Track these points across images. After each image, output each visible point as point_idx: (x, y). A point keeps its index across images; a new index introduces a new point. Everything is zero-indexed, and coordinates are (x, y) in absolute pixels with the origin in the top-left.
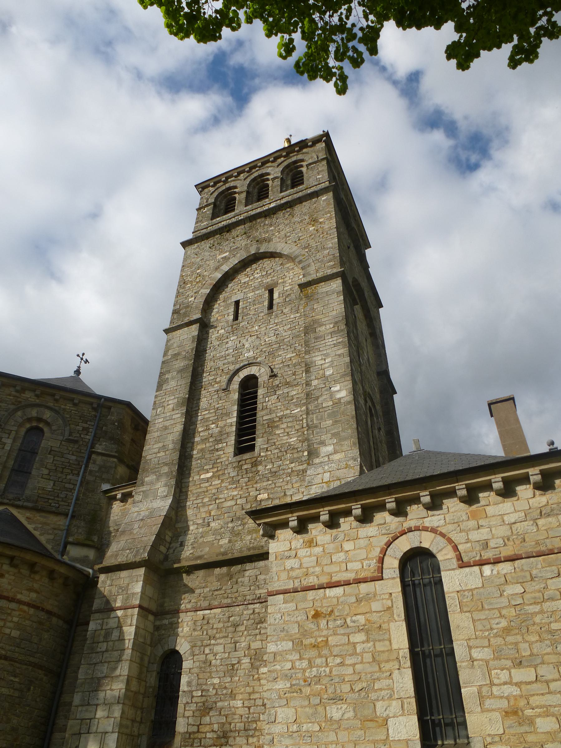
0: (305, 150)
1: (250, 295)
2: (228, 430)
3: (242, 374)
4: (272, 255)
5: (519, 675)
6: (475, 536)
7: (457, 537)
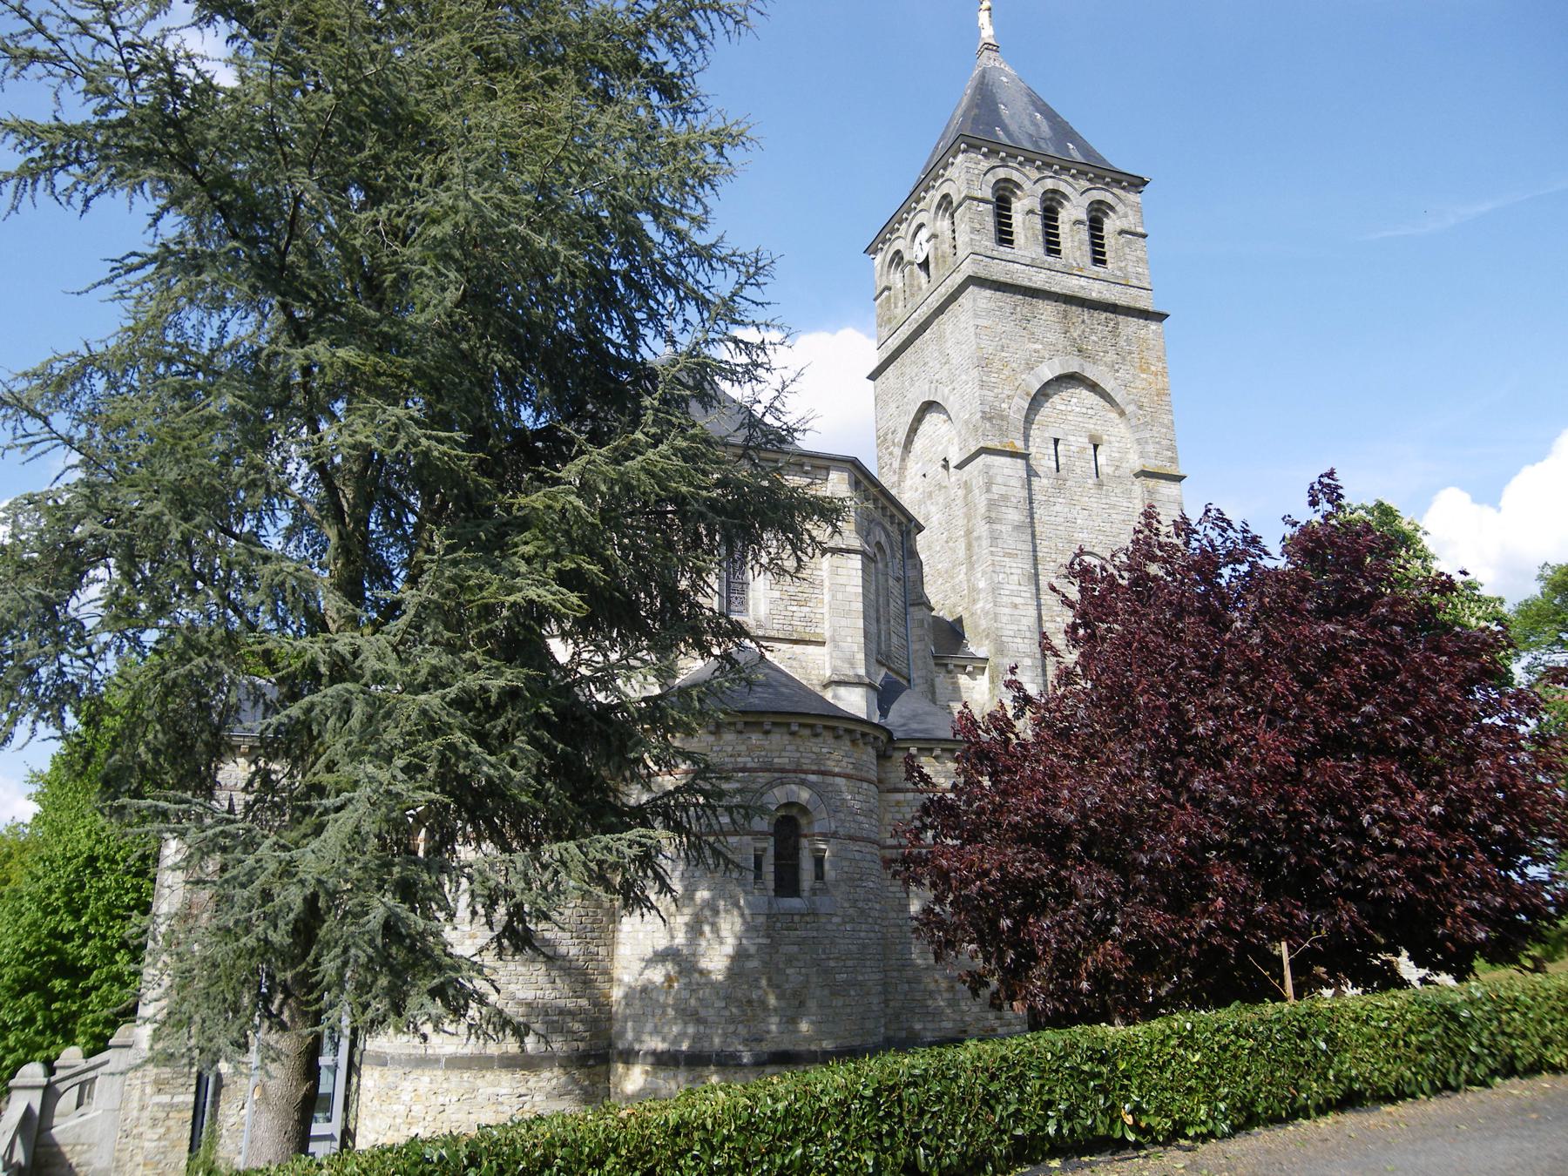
1: (1071, 438)
4: (1093, 387)
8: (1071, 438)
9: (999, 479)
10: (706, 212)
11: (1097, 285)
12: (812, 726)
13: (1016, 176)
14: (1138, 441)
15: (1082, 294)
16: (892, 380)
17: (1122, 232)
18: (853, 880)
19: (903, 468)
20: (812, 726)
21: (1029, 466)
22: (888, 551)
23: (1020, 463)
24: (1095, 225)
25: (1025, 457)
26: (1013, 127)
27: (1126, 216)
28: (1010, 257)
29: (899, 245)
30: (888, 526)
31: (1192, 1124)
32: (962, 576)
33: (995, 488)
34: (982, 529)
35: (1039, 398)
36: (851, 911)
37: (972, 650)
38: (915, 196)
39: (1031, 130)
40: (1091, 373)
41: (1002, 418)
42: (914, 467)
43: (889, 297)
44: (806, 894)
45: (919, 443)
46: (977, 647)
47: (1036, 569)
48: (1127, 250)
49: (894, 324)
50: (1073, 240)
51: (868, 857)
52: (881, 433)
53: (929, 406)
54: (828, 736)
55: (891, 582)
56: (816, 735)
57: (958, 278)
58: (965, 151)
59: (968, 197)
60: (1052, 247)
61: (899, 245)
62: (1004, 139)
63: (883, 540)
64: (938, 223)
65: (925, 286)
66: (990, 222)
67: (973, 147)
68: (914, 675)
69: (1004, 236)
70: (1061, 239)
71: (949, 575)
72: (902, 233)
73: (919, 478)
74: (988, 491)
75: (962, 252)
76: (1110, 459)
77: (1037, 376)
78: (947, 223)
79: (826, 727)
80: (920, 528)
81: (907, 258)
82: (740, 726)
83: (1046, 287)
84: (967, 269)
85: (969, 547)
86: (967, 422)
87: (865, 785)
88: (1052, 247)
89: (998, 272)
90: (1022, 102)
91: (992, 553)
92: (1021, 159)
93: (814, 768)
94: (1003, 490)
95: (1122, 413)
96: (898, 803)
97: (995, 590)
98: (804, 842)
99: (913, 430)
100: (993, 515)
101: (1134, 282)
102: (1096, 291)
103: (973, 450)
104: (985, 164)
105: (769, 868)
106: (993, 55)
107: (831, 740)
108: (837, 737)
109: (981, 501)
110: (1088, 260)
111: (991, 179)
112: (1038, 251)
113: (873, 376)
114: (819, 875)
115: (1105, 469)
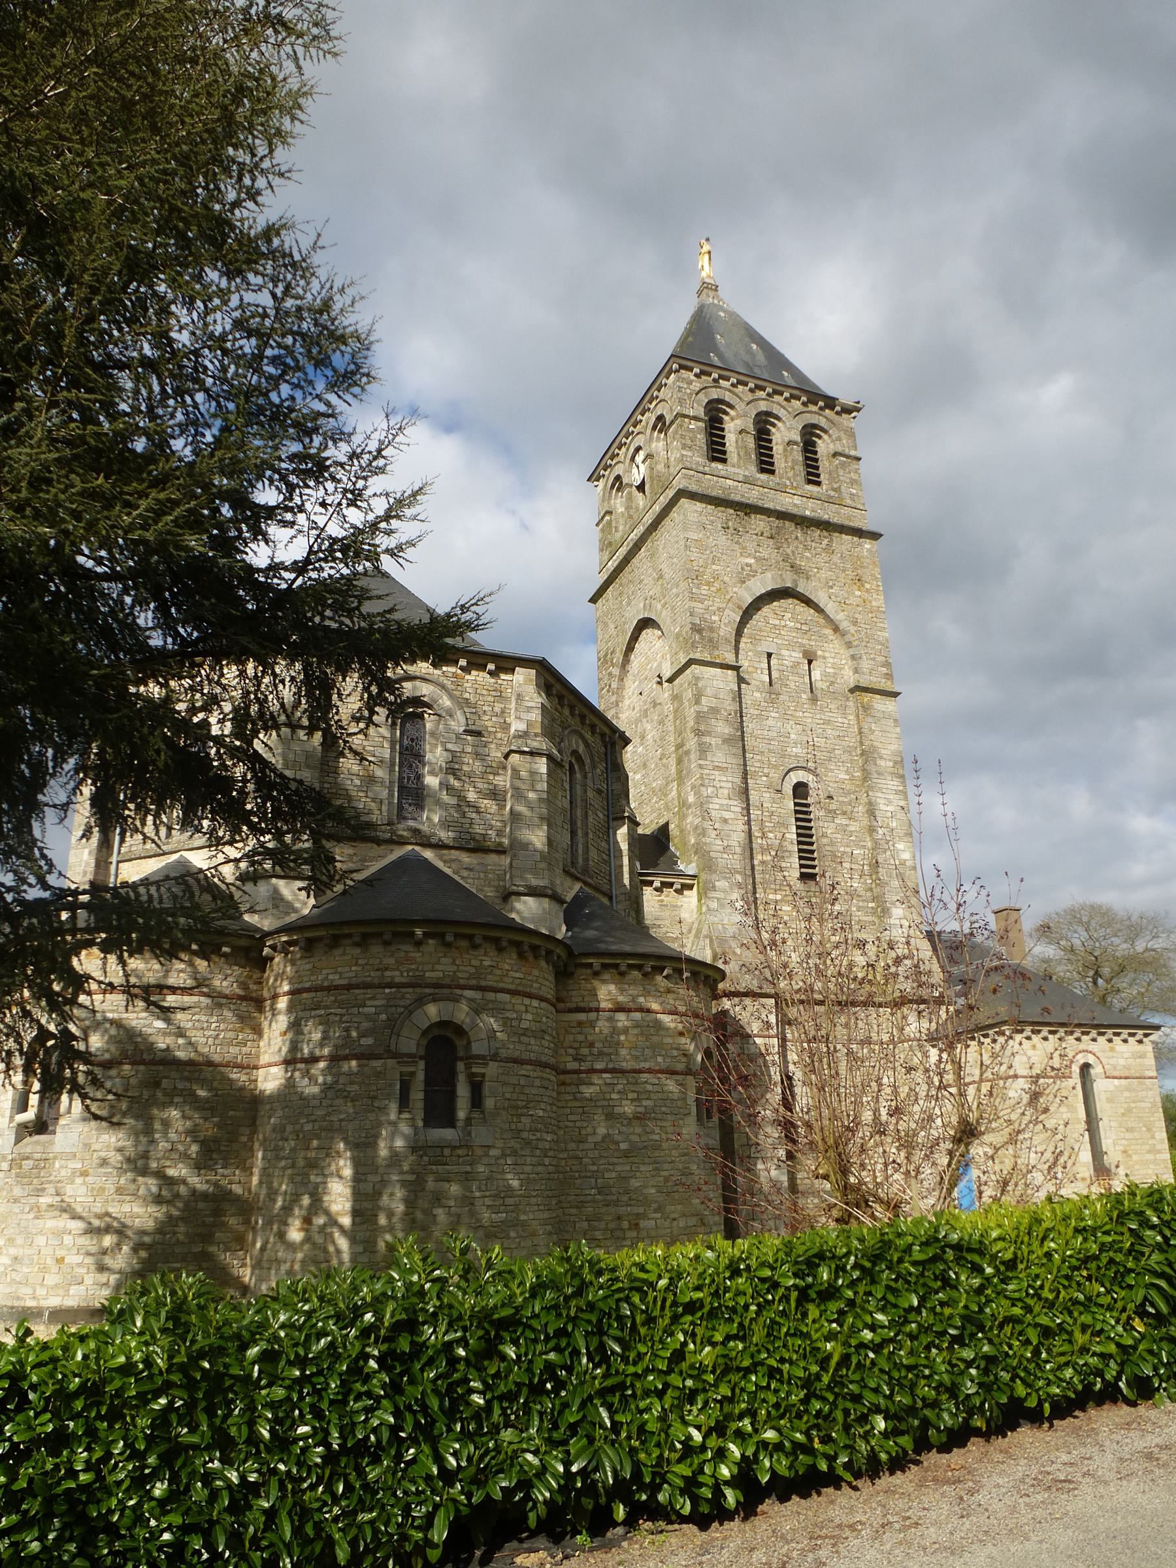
1: (785, 652)
2: (790, 848)
3: (794, 778)
4: (807, 602)
5: (1129, 1135)
6: (1112, 1061)
7: (1104, 1061)
8: (785, 652)
9: (709, 691)
11: (811, 504)
12: (470, 937)
13: (728, 397)
14: (853, 657)
15: (795, 511)
17: (835, 455)
18: (517, 1107)
19: (621, 688)
20: (616, 966)
22: (588, 761)
23: (731, 673)
25: (736, 668)
26: (728, 354)
27: (839, 439)
28: (723, 473)
29: (619, 470)
30: (588, 736)
32: (674, 793)
33: (704, 700)
34: (692, 743)
35: (748, 613)
36: (513, 1143)
37: (682, 867)
38: (632, 420)
39: (747, 358)
41: (712, 630)
44: (460, 1124)
45: (636, 659)
48: (841, 472)
49: (614, 548)
50: (786, 458)
51: (537, 1082)
52: (602, 654)
53: (646, 623)
55: (590, 794)
56: (475, 947)
57: (670, 493)
58: (677, 371)
60: (766, 464)
61: (619, 470)
62: (715, 360)
63: (581, 749)
64: (654, 445)
66: (701, 439)
69: (716, 451)
70: (775, 460)
72: (621, 457)
73: (635, 698)
74: (697, 702)
76: (825, 674)
77: (749, 589)
79: (486, 939)
81: (625, 481)
82: (387, 937)
83: (760, 503)
85: (679, 761)
86: (678, 636)
88: (766, 464)
91: (700, 766)
93: (473, 982)
94: (713, 703)
95: (836, 629)
96: (580, 1024)
98: (460, 1066)
99: (630, 648)
100: (702, 728)
101: (849, 502)
102: (810, 509)
103: (683, 661)
106: (711, 294)
107: (493, 953)
108: (500, 950)
109: (690, 712)
110: (801, 479)
112: (752, 470)
113: (594, 600)
114: (477, 1100)
115: (820, 685)
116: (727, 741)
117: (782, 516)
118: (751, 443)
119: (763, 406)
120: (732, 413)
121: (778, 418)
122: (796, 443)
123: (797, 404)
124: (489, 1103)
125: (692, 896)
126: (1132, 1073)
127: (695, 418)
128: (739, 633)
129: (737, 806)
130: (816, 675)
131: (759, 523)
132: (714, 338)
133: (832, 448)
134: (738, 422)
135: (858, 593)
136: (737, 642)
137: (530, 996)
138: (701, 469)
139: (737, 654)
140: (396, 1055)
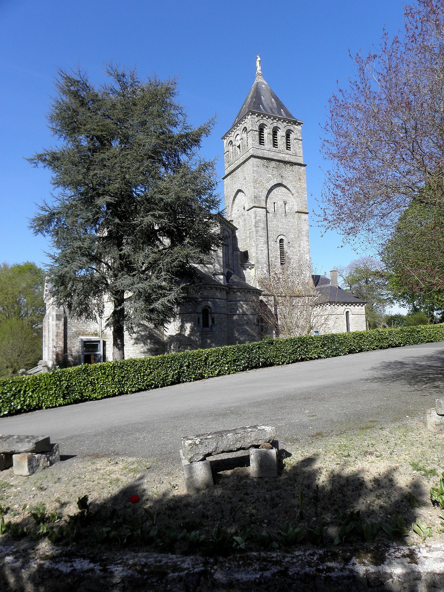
0: (294, 126)
1: (278, 202)
3: (280, 238)
4: (285, 187)
8: (278, 202)
9: (258, 215)
10: (257, 447)
11: (287, 156)
16: (229, 181)
21: (267, 211)
24: (288, 136)
26: (265, 105)
31: (104, 238)
35: (269, 192)
40: (284, 183)
41: (259, 197)
42: (235, 208)
43: (228, 155)
45: (237, 200)
46: (252, 261)
47: (268, 240)
53: (239, 191)
54: (214, 289)
59: (251, 130)
60: (275, 144)
61: (231, 139)
65: (239, 153)
66: (258, 137)
67: (253, 113)
68: (235, 270)
69: (261, 141)
71: (245, 240)
73: (236, 211)
75: (250, 146)
78: (245, 135)
80: (237, 229)
81: (234, 144)
84: (251, 152)
87: (223, 301)
88: (275, 144)
89: (260, 153)
90: (268, 94)
92: (267, 117)
94: (260, 218)
95: (293, 195)
97: (257, 246)
98: (209, 315)
99: (235, 197)
102: (287, 158)
104: (257, 119)
105: (201, 321)
111: (258, 124)
114: (213, 322)
116: (263, 229)
117: (279, 161)
118: (271, 137)
119: (275, 125)
120: (266, 127)
121: (280, 129)
122: (284, 137)
123: (285, 123)
124: (216, 322)
125: (253, 270)
126: (359, 313)
127: (256, 131)
128: (267, 197)
129: (265, 246)
130: (287, 208)
131: (273, 164)
132: (261, 97)
133: (295, 136)
134: (268, 130)
135: (299, 183)
136: (266, 200)
137: (222, 299)
138: (257, 147)
139: (266, 205)
140: (197, 313)
